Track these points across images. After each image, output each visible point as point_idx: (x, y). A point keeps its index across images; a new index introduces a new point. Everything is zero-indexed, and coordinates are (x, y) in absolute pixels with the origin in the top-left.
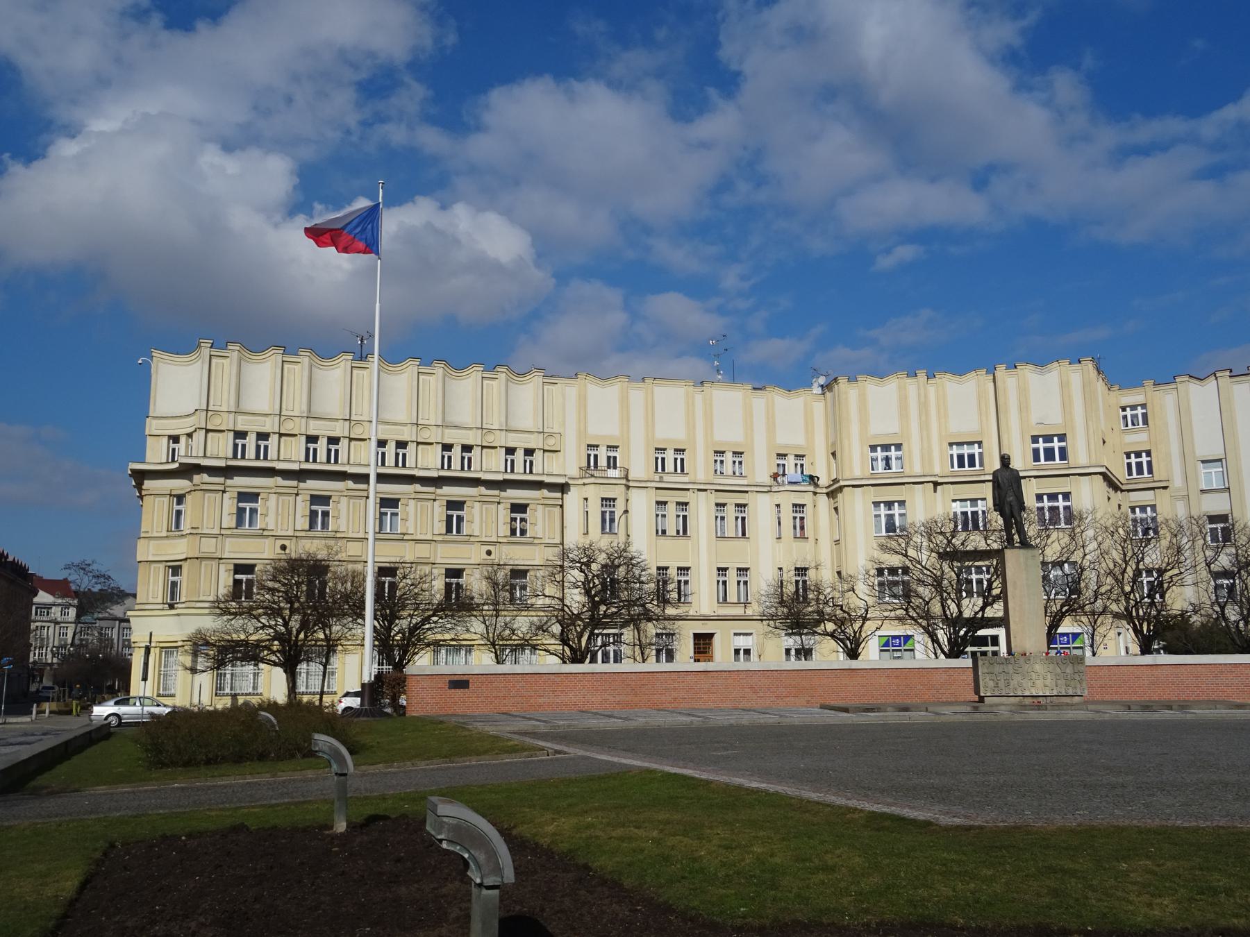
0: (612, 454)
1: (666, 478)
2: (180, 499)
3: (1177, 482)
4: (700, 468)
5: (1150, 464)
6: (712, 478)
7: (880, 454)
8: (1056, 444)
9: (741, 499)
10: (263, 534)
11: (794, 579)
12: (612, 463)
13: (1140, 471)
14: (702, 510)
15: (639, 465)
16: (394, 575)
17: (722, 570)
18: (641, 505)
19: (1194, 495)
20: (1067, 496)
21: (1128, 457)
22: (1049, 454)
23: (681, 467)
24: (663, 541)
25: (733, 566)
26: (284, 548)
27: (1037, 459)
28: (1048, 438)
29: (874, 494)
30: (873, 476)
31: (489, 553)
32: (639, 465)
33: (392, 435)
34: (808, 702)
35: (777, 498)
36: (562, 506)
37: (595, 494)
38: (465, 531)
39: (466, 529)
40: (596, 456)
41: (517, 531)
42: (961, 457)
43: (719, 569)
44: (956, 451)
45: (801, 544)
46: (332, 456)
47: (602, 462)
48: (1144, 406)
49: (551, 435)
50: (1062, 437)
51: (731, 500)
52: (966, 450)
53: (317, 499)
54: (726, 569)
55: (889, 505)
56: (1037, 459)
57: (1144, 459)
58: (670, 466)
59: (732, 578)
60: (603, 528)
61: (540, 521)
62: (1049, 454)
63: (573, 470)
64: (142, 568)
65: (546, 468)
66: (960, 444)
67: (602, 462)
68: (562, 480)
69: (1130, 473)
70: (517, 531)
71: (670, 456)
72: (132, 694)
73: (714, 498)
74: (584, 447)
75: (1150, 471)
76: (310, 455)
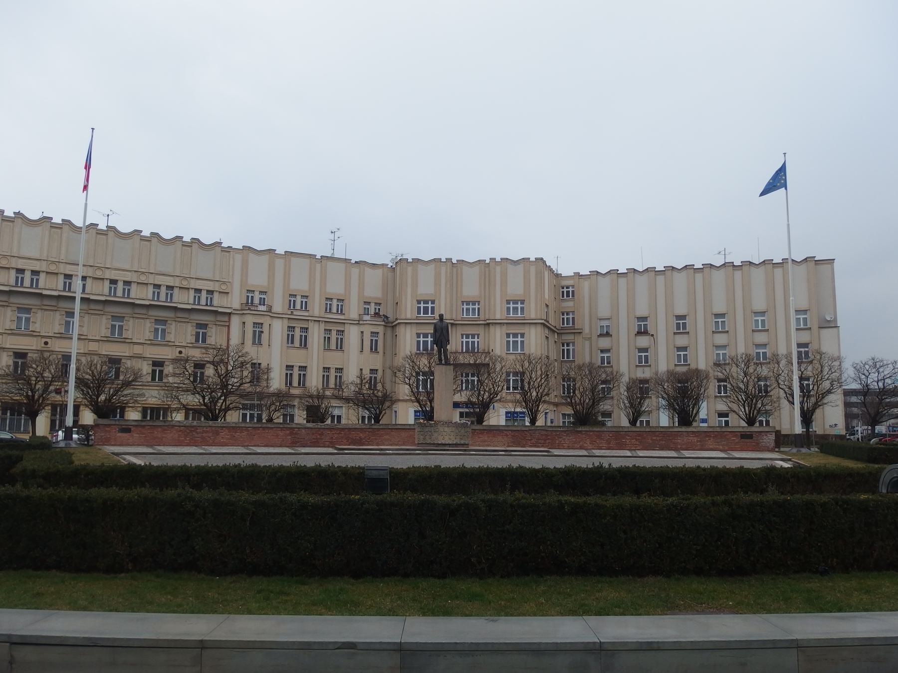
0: (263, 296)
2: (205, 326)
3: (587, 330)
5: (573, 318)
6: (323, 314)
8: (519, 306)
10: (33, 334)
11: (369, 375)
12: (262, 302)
14: (316, 335)
16: (162, 366)
17: (326, 369)
18: (278, 330)
19: (594, 337)
20: (523, 335)
21: (563, 314)
22: (426, 310)
23: (305, 306)
24: (328, 353)
25: (297, 364)
26: (180, 352)
27: (419, 313)
28: (426, 302)
29: (505, 330)
30: (417, 318)
31: (46, 343)
33: (121, 277)
34: (322, 434)
35: (362, 328)
36: (229, 326)
37: (250, 320)
38: (208, 342)
40: (252, 297)
43: (287, 366)
45: (374, 355)
46: (34, 283)
47: (256, 301)
48: (573, 286)
49: (224, 283)
50: (433, 302)
51: (298, 325)
53: (200, 326)
54: (329, 368)
56: (419, 313)
58: (298, 306)
59: (333, 374)
60: (371, 349)
61: (215, 337)
62: (426, 310)
63: (236, 305)
67: (256, 301)
68: (229, 311)
71: (299, 300)
73: (323, 326)
74: (244, 291)
76: (19, 281)
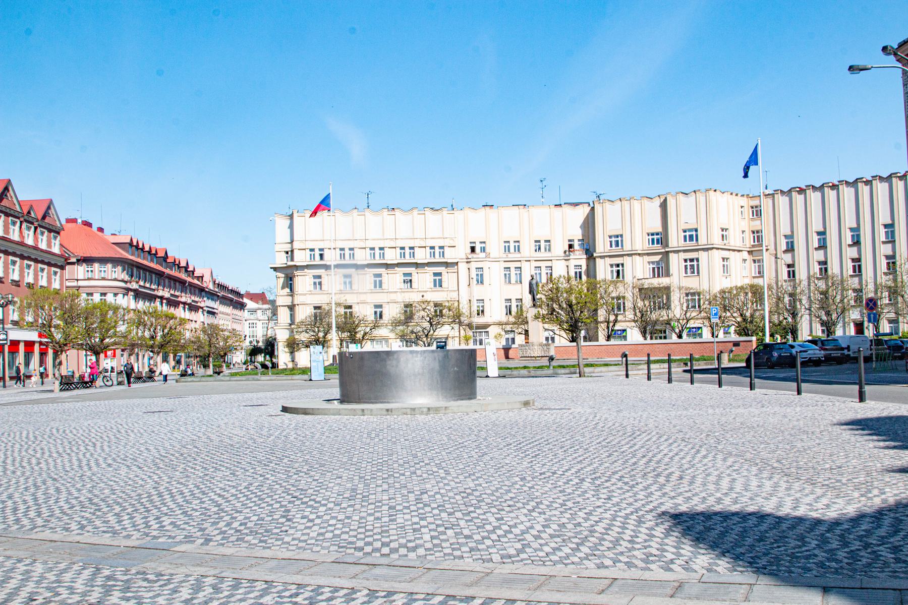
1: (510, 255)
4: (528, 249)
7: (613, 239)
9: (518, 264)
13: (617, 245)
15: (495, 249)
23: (518, 249)
32: (495, 249)
39: (384, 286)
41: (438, 283)
42: (653, 240)
44: (650, 237)
51: (512, 265)
52: (655, 237)
55: (618, 266)
57: (694, 233)
58: (512, 250)
64: (598, 260)
65: (450, 256)
66: (653, 234)
68: (456, 261)
69: (611, 246)
70: (438, 283)
71: (512, 245)
72: (598, 279)
75: (697, 240)
